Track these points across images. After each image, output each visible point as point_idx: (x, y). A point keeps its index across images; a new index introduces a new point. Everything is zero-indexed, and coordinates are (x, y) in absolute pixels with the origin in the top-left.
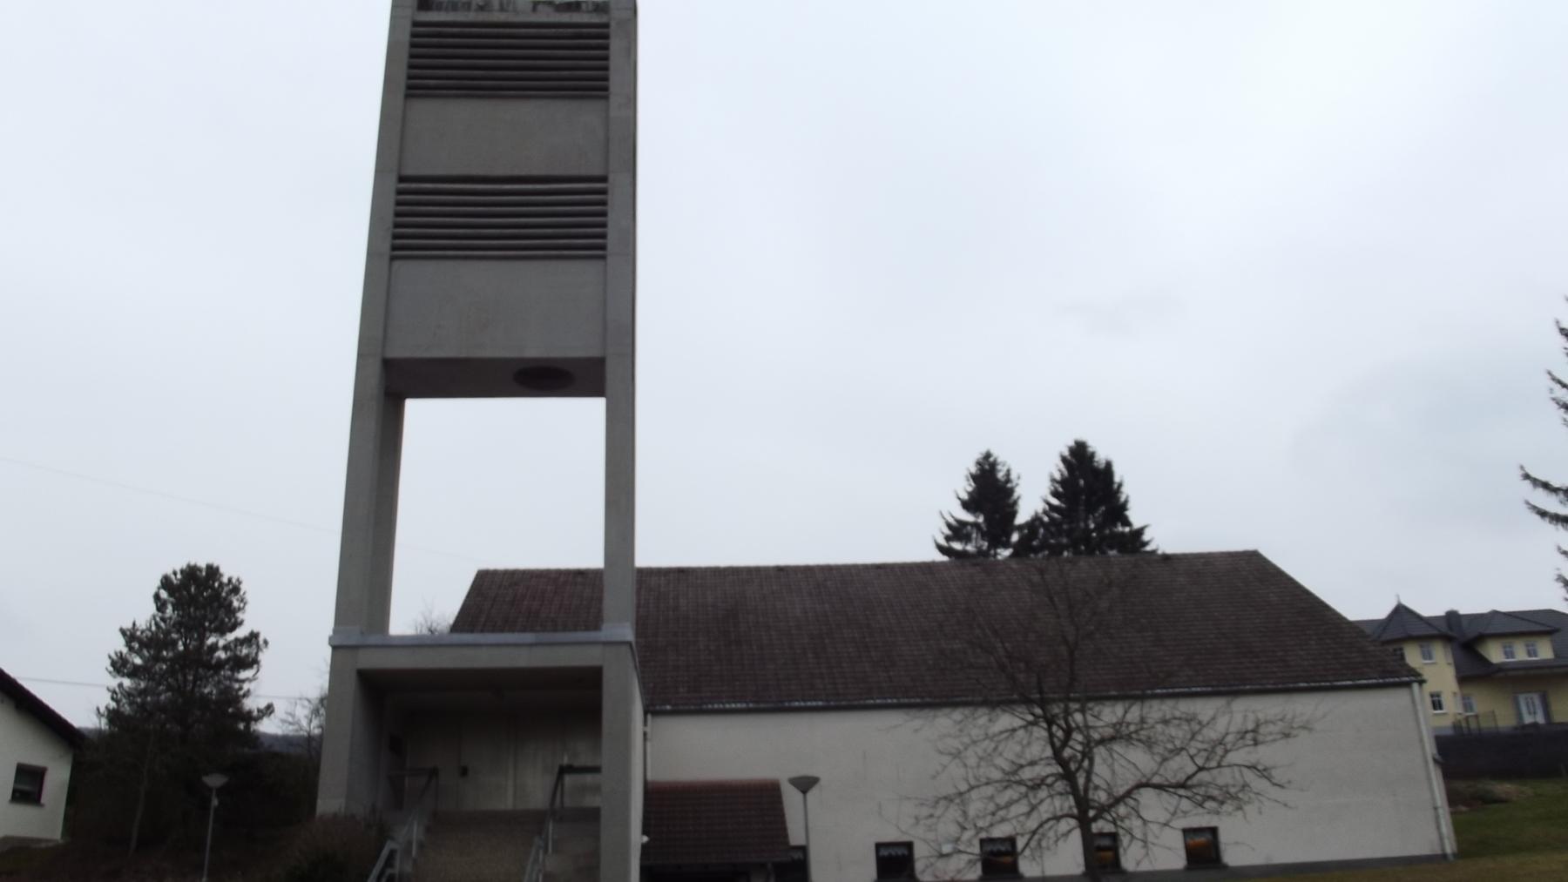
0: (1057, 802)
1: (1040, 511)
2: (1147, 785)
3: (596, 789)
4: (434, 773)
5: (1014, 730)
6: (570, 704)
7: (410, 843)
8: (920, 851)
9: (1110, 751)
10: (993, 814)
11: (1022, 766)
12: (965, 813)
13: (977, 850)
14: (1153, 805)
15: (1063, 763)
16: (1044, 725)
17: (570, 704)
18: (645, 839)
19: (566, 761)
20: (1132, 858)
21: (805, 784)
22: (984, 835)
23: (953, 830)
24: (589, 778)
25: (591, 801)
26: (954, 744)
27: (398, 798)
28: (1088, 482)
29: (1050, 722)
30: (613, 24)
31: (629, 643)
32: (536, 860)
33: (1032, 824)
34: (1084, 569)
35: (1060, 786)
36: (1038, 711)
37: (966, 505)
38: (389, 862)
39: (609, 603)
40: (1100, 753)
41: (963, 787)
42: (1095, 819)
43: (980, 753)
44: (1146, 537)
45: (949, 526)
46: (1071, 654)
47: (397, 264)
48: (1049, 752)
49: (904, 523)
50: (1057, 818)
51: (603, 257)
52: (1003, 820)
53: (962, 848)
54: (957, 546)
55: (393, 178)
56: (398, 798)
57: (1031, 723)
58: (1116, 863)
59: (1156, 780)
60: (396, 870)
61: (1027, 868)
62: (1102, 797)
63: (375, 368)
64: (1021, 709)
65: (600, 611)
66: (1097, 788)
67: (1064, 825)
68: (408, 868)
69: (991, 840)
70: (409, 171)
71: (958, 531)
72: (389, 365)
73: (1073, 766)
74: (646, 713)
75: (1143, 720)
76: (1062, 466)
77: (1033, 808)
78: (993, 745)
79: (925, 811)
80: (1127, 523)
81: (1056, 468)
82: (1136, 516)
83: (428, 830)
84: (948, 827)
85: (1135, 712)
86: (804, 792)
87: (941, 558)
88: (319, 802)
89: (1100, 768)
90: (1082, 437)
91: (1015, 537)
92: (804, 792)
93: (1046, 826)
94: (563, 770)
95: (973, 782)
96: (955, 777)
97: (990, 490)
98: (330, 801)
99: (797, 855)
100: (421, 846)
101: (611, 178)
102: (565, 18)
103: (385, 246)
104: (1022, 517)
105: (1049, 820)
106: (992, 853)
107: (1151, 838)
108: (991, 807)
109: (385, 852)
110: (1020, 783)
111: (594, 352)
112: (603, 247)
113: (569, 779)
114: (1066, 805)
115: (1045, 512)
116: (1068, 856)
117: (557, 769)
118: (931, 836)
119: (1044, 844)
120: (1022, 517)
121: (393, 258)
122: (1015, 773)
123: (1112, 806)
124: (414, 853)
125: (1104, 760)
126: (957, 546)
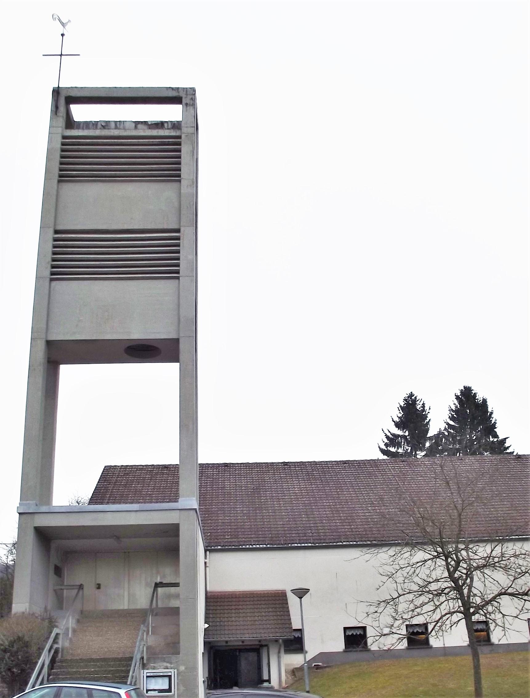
0: (451, 603)
1: (443, 429)
2: (505, 594)
3: (177, 596)
4: (81, 587)
5: (426, 561)
6: (164, 544)
7: (67, 629)
8: (370, 632)
9: (483, 573)
10: (413, 611)
11: (430, 583)
12: (396, 611)
13: (404, 632)
14: (508, 605)
15: (455, 581)
16: (443, 558)
17: (164, 544)
18: (207, 626)
19: (158, 580)
20: (497, 636)
21: (301, 593)
22: (408, 623)
23: (390, 621)
24: (173, 590)
25: (174, 603)
26: (390, 569)
27: (60, 602)
28: (472, 411)
29: (447, 556)
30: (183, 136)
31: (195, 509)
32: (142, 639)
33: (437, 616)
34: (468, 464)
35: (453, 594)
36: (439, 549)
37: (398, 425)
38: (55, 641)
39: (183, 486)
40: (477, 575)
41: (395, 595)
42: (474, 614)
43: (405, 575)
44: (507, 445)
45: (387, 437)
46: (460, 515)
47: (54, 283)
48: (446, 574)
49: (361, 435)
50: (452, 613)
51: (178, 278)
52: (419, 614)
53: (394, 631)
54: (393, 449)
55: (51, 231)
56: (60, 602)
57: (435, 557)
58: (488, 639)
59: (510, 591)
60: (59, 645)
61: (434, 642)
62: (478, 600)
63: (41, 345)
64: (429, 548)
65: (178, 490)
66: (475, 595)
67: (456, 617)
68: (67, 644)
69: (412, 626)
70: (60, 227)
71: (392, 440)
72: (49, 344)
73: (460, 582)
74: (206, 551)
75: (503, 555)
76: (456, 402)
77: (437, 607)
78: (413, 569)
79: (373, 609)
80: (496, 436)
81: (453, 403)
82: (501, 432)
83: (78, 621)
84: (386, 618)
85: (498, 551)
86: (301, 598)
87: (382, 457)
88: (13, 605)
89: (477, 583)
90: (468, 385)
91: (428, 444)
92: (301, 598)
93: (445, 618)
94: (157, 585)
95: (401, 592)
96: (389, 590)
97: (412, 415)
98: (20, 604)
99: (297, 635)
100: (74, 631)
101: (182, 230)
102: (155, 132)
103: (47, 273)
104: (432, 432)
105: (446, 614)
106: (413, 633)
107: (507, 625)
108: (412, 607)
109: (53, 635)
110: (429, 592)
111: (173, 335)
112: (178, 272)
113: (160, 590)
114: (457, 605)
115: (445, 429)
116: (457, 636)
117: (153, 585)
118: (376, 624)
119: (444, 628)
120: (432, 432)
121: (52, 280)
122: (426, 586)
123: (483, 606)
124: (70, 636)
125: (480, 579)
126: (393, 449)
